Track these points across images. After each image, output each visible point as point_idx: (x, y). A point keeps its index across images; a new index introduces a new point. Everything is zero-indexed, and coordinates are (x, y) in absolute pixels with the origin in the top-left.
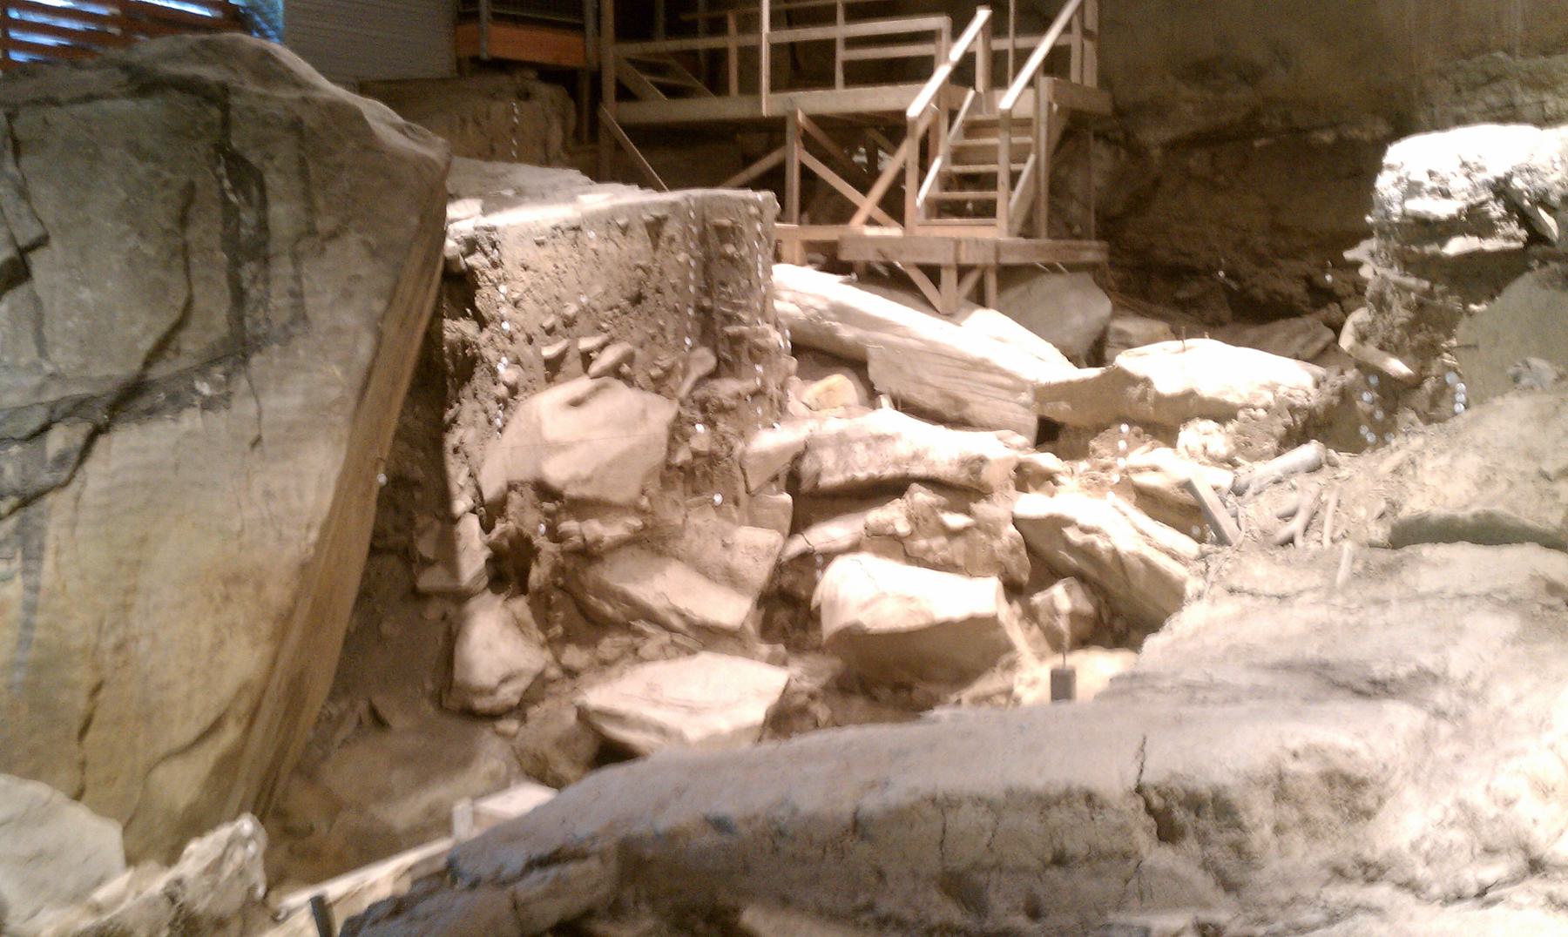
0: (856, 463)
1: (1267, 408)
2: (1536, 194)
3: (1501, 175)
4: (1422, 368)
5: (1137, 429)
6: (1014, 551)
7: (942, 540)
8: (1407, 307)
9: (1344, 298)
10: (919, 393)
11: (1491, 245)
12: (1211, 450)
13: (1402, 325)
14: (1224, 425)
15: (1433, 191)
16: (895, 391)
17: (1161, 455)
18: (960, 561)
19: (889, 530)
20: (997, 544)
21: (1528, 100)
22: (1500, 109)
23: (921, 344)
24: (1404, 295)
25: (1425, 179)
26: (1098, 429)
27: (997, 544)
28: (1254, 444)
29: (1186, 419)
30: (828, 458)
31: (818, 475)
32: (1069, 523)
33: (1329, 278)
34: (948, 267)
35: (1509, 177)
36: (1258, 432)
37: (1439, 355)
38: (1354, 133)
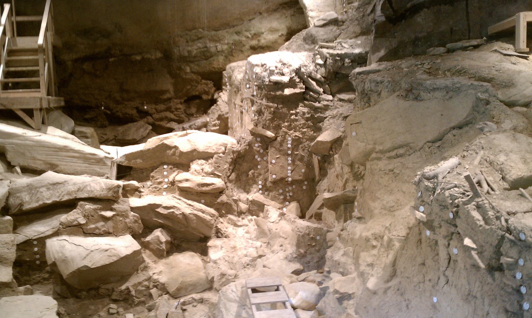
0: (44, 197)
1: (224, 153)
2: (308, 74)
3: (297, 67)
5: (170, 167)
6: (136, 222)
7: (102, 223)
8: (270, 113)
9: (153, 114)
10: (34, 164)
11: (297, 91)
12: (205, 170)
13: (269, 120)
15: (277, 73)
16: (21, 164)
17: (183, 175)
18: (111, 231)
19: (75, 223)
20: (127, 220)
21: (211, 45)
22: (203, 48)
23: (32, 143)
26: (153, 169)
27: (127, 220)
28: (222, 167)
29: (192, 161)
30: (26, 197)
31: (21, 205)
32: (159, 206)
34: (37, 109)
35: (300, 68)
36: (222, 162)
37: (281, 128)
38: (148, 56)
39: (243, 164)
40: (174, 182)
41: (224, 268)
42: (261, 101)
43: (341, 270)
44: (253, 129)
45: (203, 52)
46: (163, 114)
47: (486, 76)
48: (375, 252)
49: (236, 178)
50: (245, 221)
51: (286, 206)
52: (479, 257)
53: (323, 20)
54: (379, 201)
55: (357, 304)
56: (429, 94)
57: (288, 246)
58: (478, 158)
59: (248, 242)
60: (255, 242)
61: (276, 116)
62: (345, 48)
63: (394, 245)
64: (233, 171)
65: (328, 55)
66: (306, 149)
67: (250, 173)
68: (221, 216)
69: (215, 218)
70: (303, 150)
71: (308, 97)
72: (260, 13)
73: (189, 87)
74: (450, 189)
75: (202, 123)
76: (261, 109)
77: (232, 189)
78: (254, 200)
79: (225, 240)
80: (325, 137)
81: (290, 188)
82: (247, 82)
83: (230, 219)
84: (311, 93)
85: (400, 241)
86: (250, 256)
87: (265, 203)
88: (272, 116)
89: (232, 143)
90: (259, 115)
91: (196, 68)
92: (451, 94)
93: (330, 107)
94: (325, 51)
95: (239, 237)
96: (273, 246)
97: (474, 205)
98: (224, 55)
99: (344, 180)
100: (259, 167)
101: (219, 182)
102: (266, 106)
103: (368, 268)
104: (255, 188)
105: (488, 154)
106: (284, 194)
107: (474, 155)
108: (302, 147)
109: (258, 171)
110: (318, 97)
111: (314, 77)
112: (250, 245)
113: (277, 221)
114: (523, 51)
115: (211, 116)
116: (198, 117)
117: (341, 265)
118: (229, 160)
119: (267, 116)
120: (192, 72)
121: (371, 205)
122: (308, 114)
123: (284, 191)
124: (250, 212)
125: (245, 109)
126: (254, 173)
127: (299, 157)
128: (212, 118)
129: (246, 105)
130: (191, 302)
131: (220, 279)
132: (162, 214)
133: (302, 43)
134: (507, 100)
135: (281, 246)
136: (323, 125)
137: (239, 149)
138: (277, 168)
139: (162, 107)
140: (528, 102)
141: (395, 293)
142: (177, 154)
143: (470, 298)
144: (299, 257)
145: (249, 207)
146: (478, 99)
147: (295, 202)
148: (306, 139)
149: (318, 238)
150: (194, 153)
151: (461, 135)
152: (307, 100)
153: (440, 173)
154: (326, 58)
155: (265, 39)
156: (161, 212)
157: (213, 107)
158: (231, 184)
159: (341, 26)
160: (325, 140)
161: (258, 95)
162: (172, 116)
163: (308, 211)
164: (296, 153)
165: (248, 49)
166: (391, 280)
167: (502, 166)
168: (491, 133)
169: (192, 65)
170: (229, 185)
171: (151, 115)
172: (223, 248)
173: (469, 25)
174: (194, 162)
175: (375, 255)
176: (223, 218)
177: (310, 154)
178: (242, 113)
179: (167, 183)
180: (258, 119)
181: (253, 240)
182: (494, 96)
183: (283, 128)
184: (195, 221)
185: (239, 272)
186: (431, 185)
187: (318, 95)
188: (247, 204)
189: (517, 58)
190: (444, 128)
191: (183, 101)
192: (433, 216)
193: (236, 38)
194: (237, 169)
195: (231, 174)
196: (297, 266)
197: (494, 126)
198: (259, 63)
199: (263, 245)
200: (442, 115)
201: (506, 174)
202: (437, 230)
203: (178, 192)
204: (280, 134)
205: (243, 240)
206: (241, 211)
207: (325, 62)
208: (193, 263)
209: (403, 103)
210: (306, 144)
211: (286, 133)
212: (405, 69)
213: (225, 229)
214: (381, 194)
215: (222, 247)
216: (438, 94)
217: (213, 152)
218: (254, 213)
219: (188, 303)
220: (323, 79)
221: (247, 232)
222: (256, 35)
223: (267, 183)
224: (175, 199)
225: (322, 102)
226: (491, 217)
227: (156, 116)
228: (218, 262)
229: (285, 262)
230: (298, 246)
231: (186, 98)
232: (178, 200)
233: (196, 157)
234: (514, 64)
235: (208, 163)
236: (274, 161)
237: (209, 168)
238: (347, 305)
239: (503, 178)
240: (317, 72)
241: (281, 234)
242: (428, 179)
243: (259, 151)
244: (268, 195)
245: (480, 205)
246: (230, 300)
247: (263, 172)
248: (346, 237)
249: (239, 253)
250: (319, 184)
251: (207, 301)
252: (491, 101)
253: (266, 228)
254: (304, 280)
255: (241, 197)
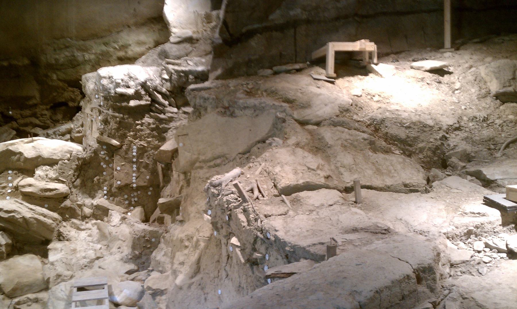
1: (69, 160)
4: (122, 142)
5: (15, 172)
8: (116, 123)
11: (143, 103)
12: (49, 176)
13: (114, 129)
14: (52, 167)
15: (123, 86)
21: (79, 54)
24: (115, 119)
25: (120, 81)
28: (66, 173)
29: (37, 166)
33: (10, 113)
36: (66, 168)
38: (15, 62)
39: (89, 170)
40: (18, 187)
41: (60, 269)
42: (107, 111)
43: (160, 269)
44: (98, 137)
45: (70, 60)
46: (28, 120)
47: (290, 97)
48: (186, 251)
49: (81, 183)
50: (89, 225)
51: (130, 211)
52: (241, 253)
53: (179, 37)
54: (195, 206)
55: (169, 299)
56: (241, 112)
57: (125, 248)
58: (260, 169)
59: (89, 244)
60: (95, 245)
61: (121, 124)
62: (190, 65)
63: (200, 245)
64: (78, 177)
65: (173, 71)
66: (151, 157)
67: (95, 179)
68: (65, 220)
69: (58, 222)
70: (148, 158)
71: (154, 109)
72: (129, 27)
73: (54, 94)
74: (228, 195)
75: (66, 129)
76: (107, 119)
77: (76, 194)
78: (98, 204)
79: (67, 243)
80: (167, 146)
81: (135, 194)
82: (97, 92)
83: (73, 223)
84: (157, 105)
85: (204, 241)
86: (88, 258)
87: (110, 207)
88: (117, 126)
89: (78, 150)
90: (106, 124)
91: (62, 76)
92: (257, 112)
93: (174, 119)
94: (170, 67)
95: (81, 240)
96: (112, 248)
97: (241, 209)
98: (91, 64)
99: (180, 186)
100: (104, 173)
101: (62, 188)
102: (113, 116)
103: (179, 266)
104: (100, 193)
105: (268, 165)
106: (129, 199)
107: (258, 166)
108: (147, 155)
109: (103, 178)
110: (163, 109)
111: (160, 91)
112: (91, 247)
113: (118, 225)
114: (330, 76)
115: (75, 122)
116: (63, 123)
117: (161, 264)
118: (74, 167)
119: (113, 125)
120: (59, 80)
121: (189, 209)
122: (154, 124)
123: (129, 196)
124: (94, 216)
125: (94, 118)
126: (100, 179)
127: (144, 164)
128: (76, 125)
129: (95, 113)
130: (26, 302)
131: (56, 280)
132: (3, 218)
133: (157, 57)
134: (301, 120)
135: (119, 248)
136: (167, 135)
137: (85, 156)
138: (122, 175)
139: (28, 112)
140: (319, 121)
141: (197, 287)
142: (22, 160)
143: (241, 289)
144: (134, 259)
145: (94, 211)
146: (277, 117)
147: (140, 207)
148: (150, 147)
149: (153, 240)
150: (39, 160)
151: (263, 148)
152: (153, 112)
153: (223, 181)
154: (172, 73)
155: (132, 51)
156: (2, 216)
157: (77, 114)
158: (76, 190)
159: (194, 43)
160: (167, 150)
161: (104, 105)
162: (37, 122)
163: (152, 216)
164: (141, 160)
165: (115, 60)
166: (195, 276)
167: (275, 176)
168: (277, 147)
169: (59, 73)
170: (73, 190)
171: (16, 120)
172: (63, 251)
173: (296, 51)
174: (39, 168)
175: (186, 254)
176: (67, 222)
177: (155, 162)
178: (92, 121)
179: (11, 188)
180: (104, 129)
181: (94, 243)
182: (290, 116)
183: (128, 137)
184: (35, 225)
185: (76, 273)
186: (216, 192)
187: (163, 107)
188: (92, 209)
189: (324, 82)
190: (251, 142)
191: (48, 107)
192: (217, 219)
193: (104, 48)
194: (82, 176)
195: (76, 180)
196: (132, 266)
197: (280, 141)
198: (107, 76)
199: (103, 247)
200: (250, 130)
201: (277, 183)
202: (221, 230)
203: (21, 197)
204: (126, 143)
205: (84, 243)
206: (85, 215)
207: (171, 77)
208: (32, 265)
209: (222, 120)
210: (151, 152)
211: (132, 142)
212: (232, 88)
213: (67, 233)
214: (198, 199)
215: (62, 250)
216: (248, 112)
217: (58, 158)
218: (98, 217)
219: (23, 302)
220: (168, 93)
221: (90, 236)
222: (124, 47)
223: (112, 189)
224: (17, 203)
225: (167, 114)
226: (252, 219)
227: (21, 121)
228: (55, 263)
229: (120, 263)
230: (134, 248)
231: (52, 104)
232: (20, 205)
233: (40, 163)
234: (319, 87)
235: (52, 169)
236: (119, 168)
237: (54, 174)
238: (160, 300)
239: (275, 186)
240: (162, 86)
241: (120, 237)
242: (215, 186)
243: (105, 158)
244: (113, 200)
245: (246, 209)
246: (58, 299)
247: (108, 178)
248: (168, 239)
249: (78, 255)
250: (163, 190)
251: (41, 300)
252: (286, 120)
253: (106, 232)
254: (133, 280)
255: (86, 202)
